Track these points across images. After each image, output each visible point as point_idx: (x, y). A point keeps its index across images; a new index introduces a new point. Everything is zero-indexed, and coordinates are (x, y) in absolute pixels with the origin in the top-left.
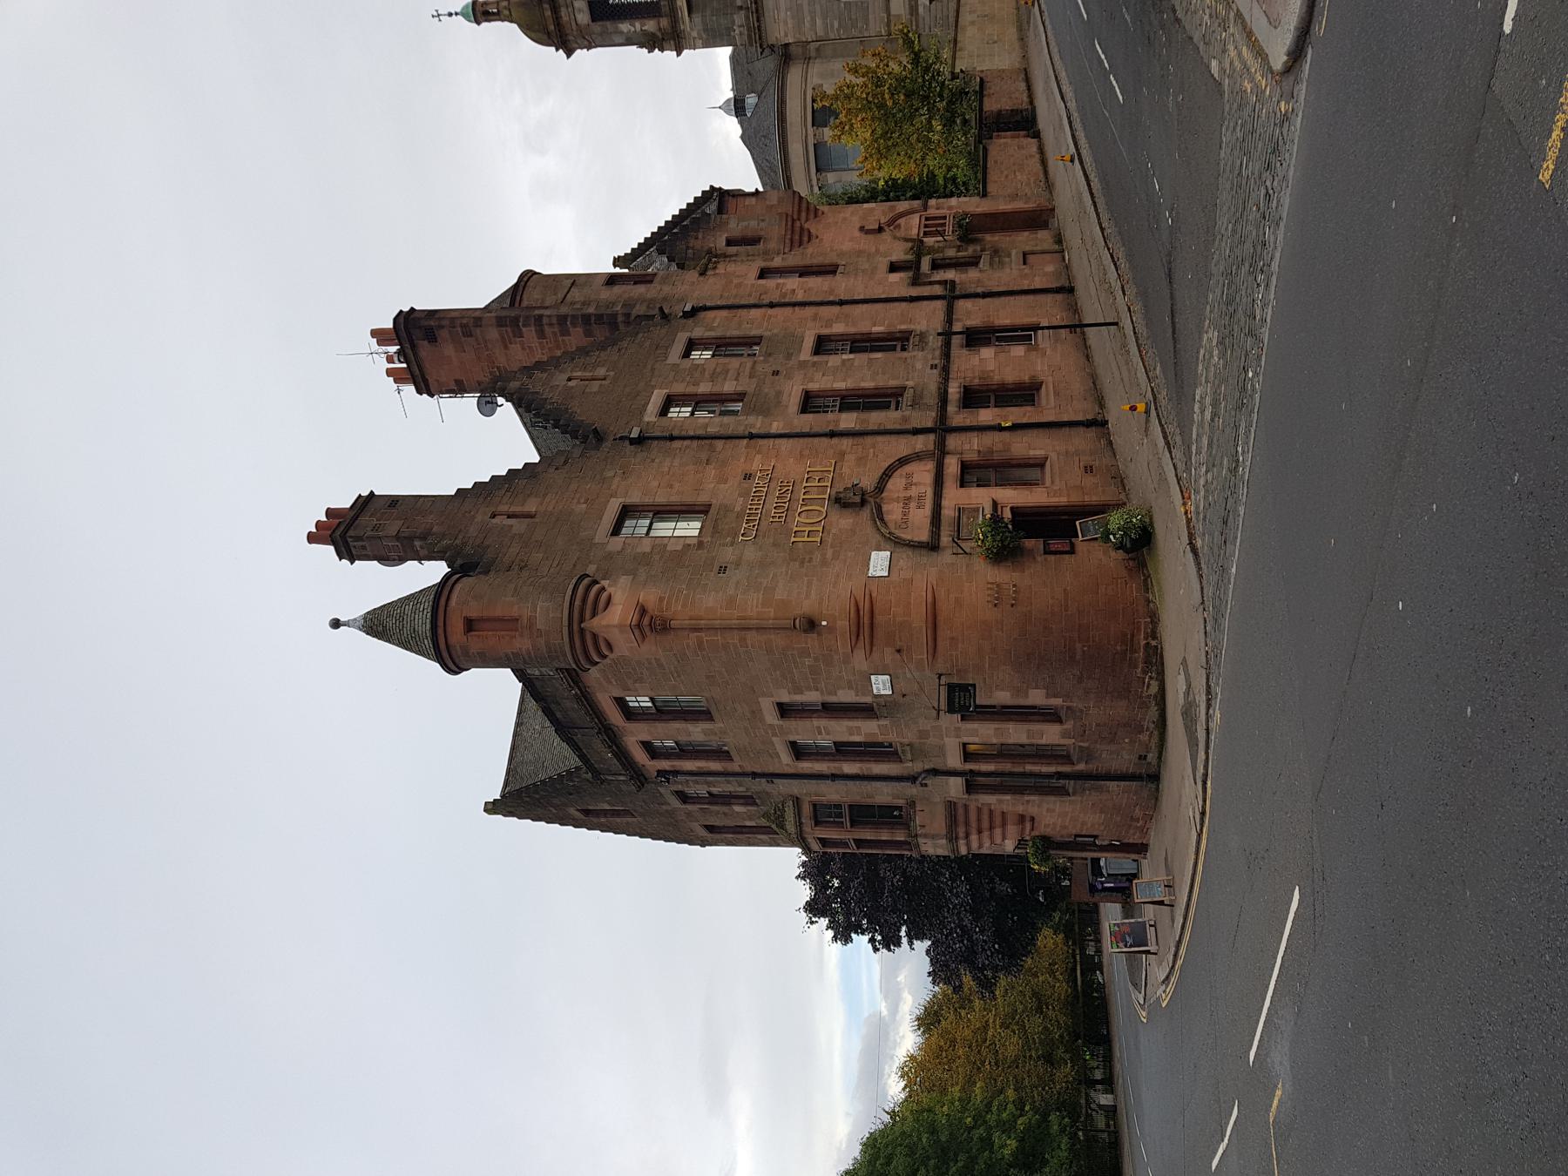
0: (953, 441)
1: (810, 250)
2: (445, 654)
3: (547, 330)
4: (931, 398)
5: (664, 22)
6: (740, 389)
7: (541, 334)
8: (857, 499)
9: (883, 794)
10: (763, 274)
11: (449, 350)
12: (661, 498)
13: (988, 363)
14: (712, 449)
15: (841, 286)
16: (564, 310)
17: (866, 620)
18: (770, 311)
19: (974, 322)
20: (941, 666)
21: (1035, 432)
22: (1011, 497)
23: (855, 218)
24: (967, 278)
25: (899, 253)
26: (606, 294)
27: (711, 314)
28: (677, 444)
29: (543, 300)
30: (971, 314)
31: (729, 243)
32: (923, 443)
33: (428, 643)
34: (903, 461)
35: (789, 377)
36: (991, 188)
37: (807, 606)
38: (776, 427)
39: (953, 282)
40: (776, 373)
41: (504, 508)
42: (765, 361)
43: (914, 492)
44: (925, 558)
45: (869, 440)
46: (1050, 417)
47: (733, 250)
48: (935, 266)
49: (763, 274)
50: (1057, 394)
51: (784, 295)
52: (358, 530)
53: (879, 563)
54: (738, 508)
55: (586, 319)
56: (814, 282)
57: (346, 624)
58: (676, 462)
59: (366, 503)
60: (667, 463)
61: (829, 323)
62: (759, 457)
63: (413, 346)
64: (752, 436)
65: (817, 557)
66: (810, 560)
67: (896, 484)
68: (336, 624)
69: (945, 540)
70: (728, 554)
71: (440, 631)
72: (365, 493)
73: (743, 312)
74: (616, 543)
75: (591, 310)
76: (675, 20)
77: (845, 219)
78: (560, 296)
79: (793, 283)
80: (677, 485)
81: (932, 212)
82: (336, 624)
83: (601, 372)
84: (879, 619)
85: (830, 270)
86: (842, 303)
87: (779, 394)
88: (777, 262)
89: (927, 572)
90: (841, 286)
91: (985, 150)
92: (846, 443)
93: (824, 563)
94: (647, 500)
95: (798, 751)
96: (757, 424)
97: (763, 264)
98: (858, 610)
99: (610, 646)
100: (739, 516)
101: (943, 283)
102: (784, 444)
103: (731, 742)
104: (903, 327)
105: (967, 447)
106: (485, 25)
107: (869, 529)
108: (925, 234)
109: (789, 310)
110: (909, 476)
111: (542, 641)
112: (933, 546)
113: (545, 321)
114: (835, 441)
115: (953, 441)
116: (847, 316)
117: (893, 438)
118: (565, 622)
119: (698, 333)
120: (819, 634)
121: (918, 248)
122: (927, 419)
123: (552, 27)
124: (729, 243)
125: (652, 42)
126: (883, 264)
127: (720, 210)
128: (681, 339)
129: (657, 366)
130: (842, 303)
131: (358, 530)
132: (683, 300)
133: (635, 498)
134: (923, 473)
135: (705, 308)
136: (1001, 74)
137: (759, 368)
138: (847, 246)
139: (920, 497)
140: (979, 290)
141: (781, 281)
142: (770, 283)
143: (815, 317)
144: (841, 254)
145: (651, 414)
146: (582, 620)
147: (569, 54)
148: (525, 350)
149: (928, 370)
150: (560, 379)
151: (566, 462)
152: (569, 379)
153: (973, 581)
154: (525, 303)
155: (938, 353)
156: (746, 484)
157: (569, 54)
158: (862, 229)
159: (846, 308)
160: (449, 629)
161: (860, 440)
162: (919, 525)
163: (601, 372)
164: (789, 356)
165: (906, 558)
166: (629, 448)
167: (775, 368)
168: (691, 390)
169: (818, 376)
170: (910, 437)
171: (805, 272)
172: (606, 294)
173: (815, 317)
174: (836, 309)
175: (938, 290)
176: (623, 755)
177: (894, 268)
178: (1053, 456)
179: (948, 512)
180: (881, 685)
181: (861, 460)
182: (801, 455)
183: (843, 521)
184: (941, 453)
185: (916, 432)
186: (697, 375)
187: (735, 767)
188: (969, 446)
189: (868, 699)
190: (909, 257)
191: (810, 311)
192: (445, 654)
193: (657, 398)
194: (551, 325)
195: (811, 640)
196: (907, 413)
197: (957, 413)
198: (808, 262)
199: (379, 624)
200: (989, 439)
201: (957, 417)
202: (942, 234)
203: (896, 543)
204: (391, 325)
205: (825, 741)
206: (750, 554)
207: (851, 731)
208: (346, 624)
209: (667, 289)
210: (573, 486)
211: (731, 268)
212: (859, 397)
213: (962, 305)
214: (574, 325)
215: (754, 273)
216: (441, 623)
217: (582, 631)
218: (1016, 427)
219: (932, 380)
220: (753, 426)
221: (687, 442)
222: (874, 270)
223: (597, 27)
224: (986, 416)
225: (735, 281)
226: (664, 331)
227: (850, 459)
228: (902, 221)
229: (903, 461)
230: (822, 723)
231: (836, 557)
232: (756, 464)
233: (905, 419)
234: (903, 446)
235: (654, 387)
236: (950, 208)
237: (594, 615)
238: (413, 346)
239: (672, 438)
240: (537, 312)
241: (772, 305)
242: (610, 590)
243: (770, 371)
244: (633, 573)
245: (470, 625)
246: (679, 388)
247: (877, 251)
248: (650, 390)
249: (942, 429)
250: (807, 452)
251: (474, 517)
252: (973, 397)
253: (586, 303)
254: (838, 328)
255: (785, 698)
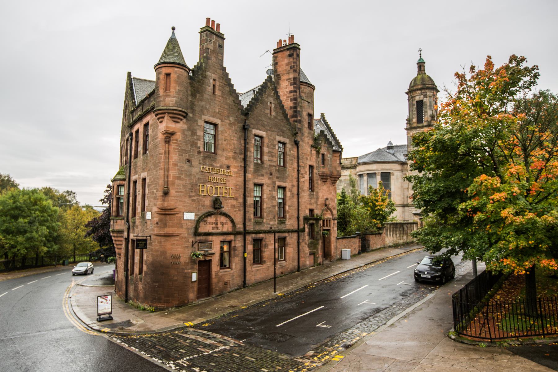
0: (240, 238)
1: (319, 182)
2: (159, 66)
3: (292, 94)
4: (258, 228)
5: (415, 125)
6: (265, 162)
7: (291, 92)
8: (216, 206)
9: (124, 213)
10: (311, 167)
11: (286, 61)
12: (220, 137)
13: (270, 246)
14: (241, 154)
15: (305, 194)
16: (299, 100)
17: (167, 212)
18: (296, 170)
19: (288, 240)
20: (153, 237)
21: (242, 265)
22: (216, 260)
23: (331, 196)
24: (306, 237)
25: (317, 212)
26: (305, 114)
27: (296, 150)
28: (243, 142)
29: (303, 92)
30: (292, 239)
31: (323, 155)
32: (240, 226)
33: (163, 61)
34: (232, 221)
35: (269, 178)
36: (340, 241)
37: (172, 192)
38: (249, 176)
39: (304, 231)
40: (271, 174)
41: (217, 83)
42: (276, 170)
43: (220, 225)
44: (192, 231)
45: (242, 208)
46: (248, 269)
47: (320, 156)
48: (312, 225)
49: (311, 167)
50: (257, 270)
51: (302, 174)
52: (212, 35)
53: (190, 216)
54: (215, 164)
55: (295, 107)
56: (307, 185)
57: (173, 33)
58: (235, 142)
59: (221, 37)
60: (235, 139)
61: (290, 191)
62: (236, 170)
63: (288, 49)
64: (245, 167)
65: (193, 194)
66: (192, 192)
67: (223, 219)
68: (173, 29)
69: (198, 238)
70: (195, 162)
71: (166, 65)
72: (225, 37)
73: (296, 161)
74: (201, 123)
75: (299, 109)
76: (416, 128)
77: (331, 193)
78: (305, 98)
79: (307, 177)
80: (225, 143)
81: (332, 222)
82: (173, 29)
83: (274, 114)
84: (168, 216)
85: (312, 188)
86: (298, 194)
87: (263, 175)
88: (315, 171)
89: (186, 232)
90: (305, 194)
91: (354, 237)
92: (241, 200)
93: (190, 197)
94: (219, 133)
95: (135, 182)
96: (251, 168)
97: (315, 167)
98: (173, 209)
99: (161, 122)
100: (212, 165)
101: (304, 228)
102: (241, 179)
103: (138, 159)
104: (288, 217)
105: (237, 242)
106: (417, 66)
107: (204, 211)
108: (324, 220)
109: (296, 177)
110: (226, 223)
111: (162, 99)
112: (196, 233)
113: (295, 94)
114: (242, 196)
115: (240, 238)
116: (293, 197)
117: (242, 216)
118: (167, 108)
119: (289, 146)
120: (162, 196)
121: (317, 220)
122: (250, 227)
123: (415, 88)
124: (323, 155)
125: (409, 121)
126: (312, 207)
127: (334, 151)
128: (287, 141)
129: (276, 133)
130: (298, 194)
131: (212, 35)
132: (302, 140)
133: (220, 128)
134: (228, 227)
135: (298, 148)
136: (384, 240)
137: (274, 168)
138: (320, 194)
139: (217, 228)
140: (301, 241)
141: (308, 173)
142: (307, 169)
143: (293, 186)
144: (317, 193)
145: (255, 131)
146: (169, 113)
147: (407, 93)
148: (285, 89)
149: (269, 226)
150: (271, 99)
151: (236, 103)
152: (271, 103)
153: (181, 249)
154: (301, 86)
155: (277, 229)
156: (225, 166)
157: (407, 93)
158: (327, 199)
159: (296, 196)
160: (167, 68)
161: (242, 205)
162: (204, 228)
163: (274, 114)
164: (278, 178)
165: (192, 226)
166: (241, 125)
167: (273, 174)
168: (265, 145)
169: (269, 188)
170: (243, 222)
171: (311, 181)
172: (305, 114)
173: (293, 186)
174: (296, 192)
175: (301, 226)
176: (135, 122)
177: (311, 211)
178: (232, 272)
179: (210, 238)
180: (148, 216)
181: (233, 206)
182: (237, 185)
183: (208, 202)
184: (236, 233)
185: (244, 224)
186: (271, 147)
187: (132, 160)
188: (238, 243)
189: (146, 210)
190: (315, 216)
191: (295, 183)
192: (159, 66)
193: (263, 133)
194: (294, 95)
195: (160, 193)
196: (253, 220)
197: (252, 238)
198: (315, 182)
199: (173, 43)
200: (241, 250)
201: (249, 238)
202: (324, 225)
203: (200, 220)
204: (295, 42)
205: (137, 193)
206: (195, 170)
207: (139, 202)
208: (173, 33)
209: (306, 134)
210: (226, 107)
211: (314, 156)
212: (47, 272)
213: (295, 236)
214: (294, 103)
215: (311, 164)
216: (169, 65)
217: (165, 113)
218: (245, 259)
219: (265, 228)
220: (250, 167)
221: (243, 145)
222: (311, 204)
223: (415, 102)
224: (250, 248)
225: (308, 158)
226: (290, 134)
227: (234, 202)
228: (329, 212)
229: (232, 221)
230: (141, 193)
231: (193, 200)
232: (233, 170)
233: (250, 220)
234: (238, 220)
235: (267, 132)
236: (333, 228)
237: (171, 117)
238: (288, 49)
239: (245, 140)
240: (298, 91)
241: (298, 171)
242: (182, 122)
243: (272, 171)
244: (189, 129)
245: (168, 75)
246: (266, 141)
247: (317, 205)
248: (266, 131)
249: (245, 233)
250: (238, 187)
251: (214, 73)
252: (258, 243)
253: (301, 107)
254: (288, 194)
255: (147, 181)
